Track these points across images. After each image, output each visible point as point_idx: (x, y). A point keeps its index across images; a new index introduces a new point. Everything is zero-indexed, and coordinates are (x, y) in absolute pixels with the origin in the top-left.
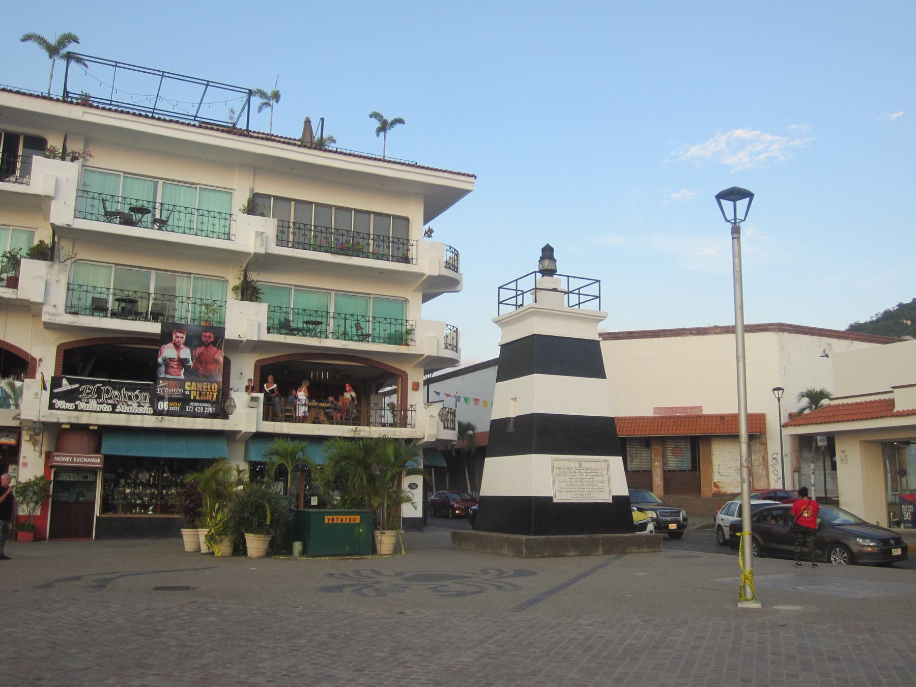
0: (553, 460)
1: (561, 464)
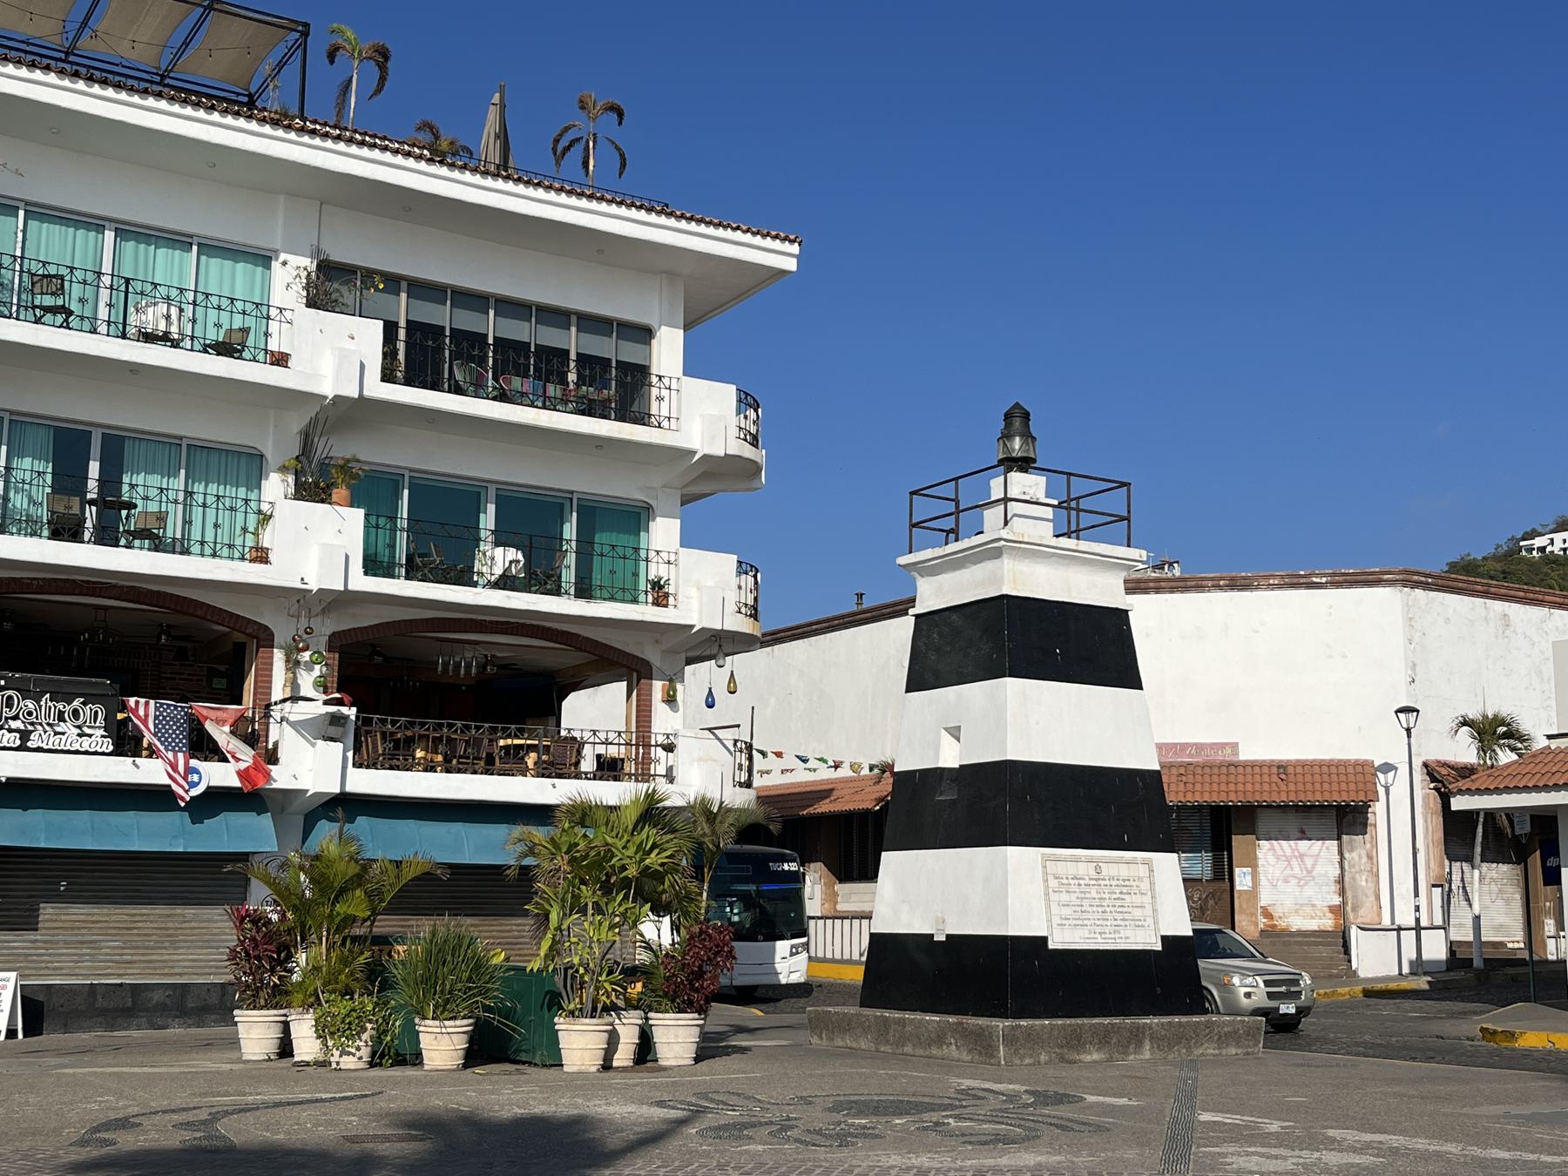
0: (1046, 859)
1: (1060, 868)
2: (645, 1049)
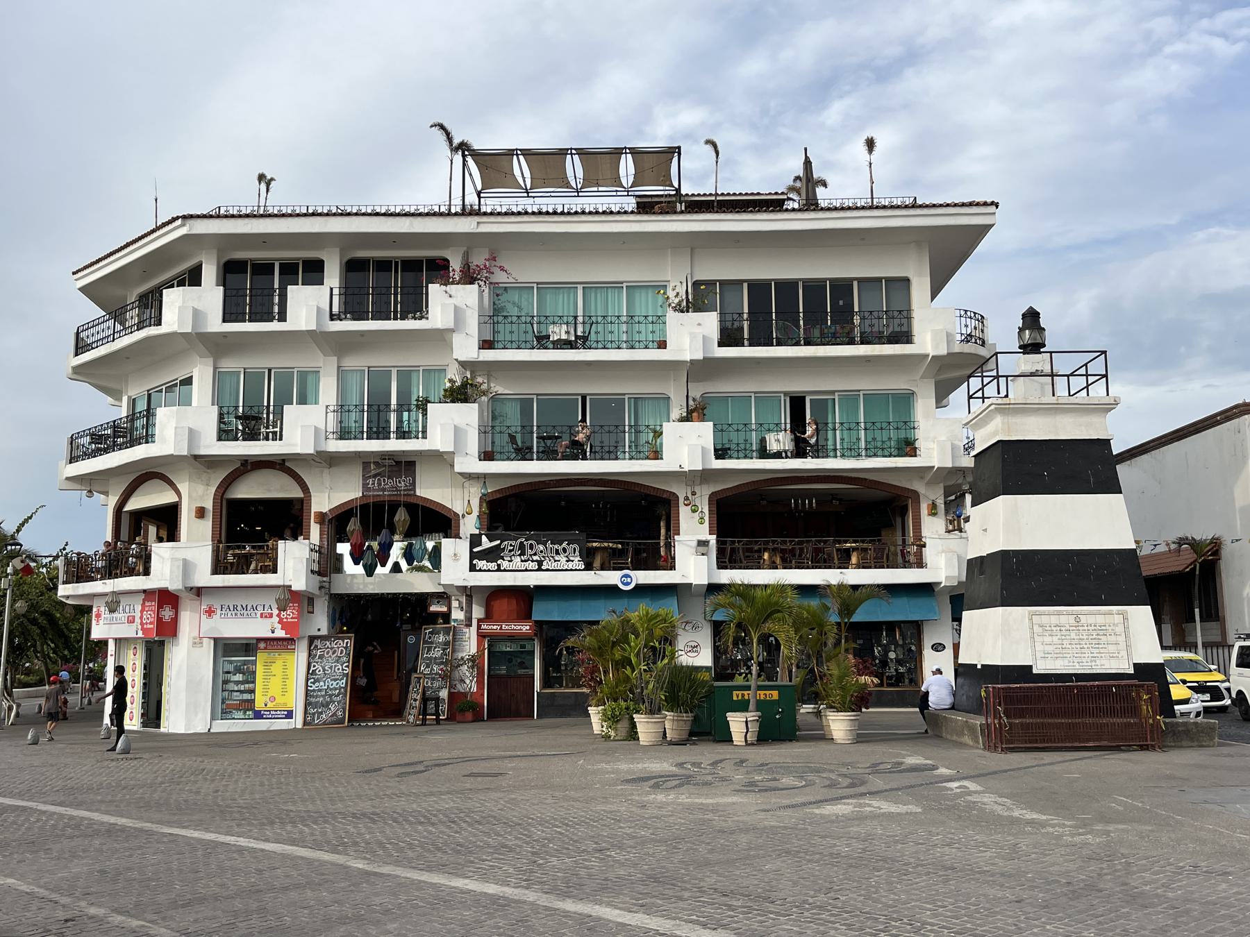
1: (1044, 619)
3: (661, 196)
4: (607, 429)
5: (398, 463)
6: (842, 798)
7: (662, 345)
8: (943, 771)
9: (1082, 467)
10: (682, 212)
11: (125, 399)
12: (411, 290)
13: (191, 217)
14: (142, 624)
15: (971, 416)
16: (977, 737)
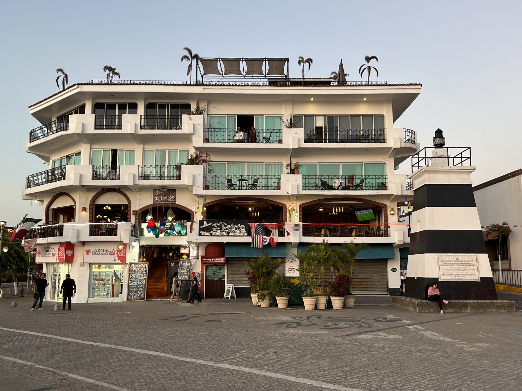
1: (444, 259)
2: (329, 305)
3: (280, 79)
4: (311, 177)
5: (169, 190)
6: (367, 332)
7: (280, 142)
8: (405, 321)
9: (459, 195)
10: (289, 86)
11: (51, 161)
12: (175, 117)
13: (82, 84)
14: (58, 257)
15: (413, 174)
16: (416, 307)
